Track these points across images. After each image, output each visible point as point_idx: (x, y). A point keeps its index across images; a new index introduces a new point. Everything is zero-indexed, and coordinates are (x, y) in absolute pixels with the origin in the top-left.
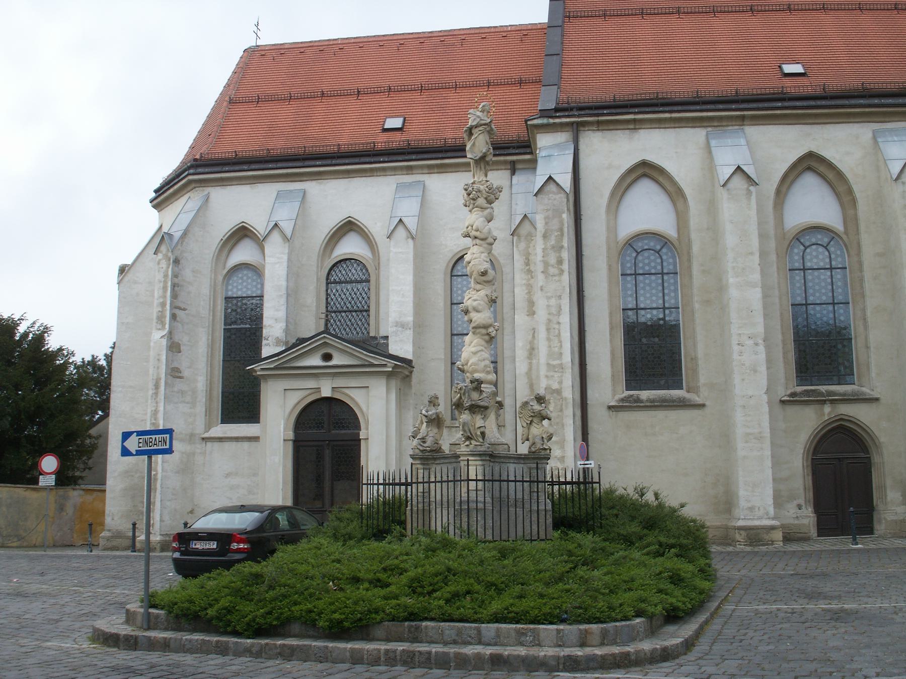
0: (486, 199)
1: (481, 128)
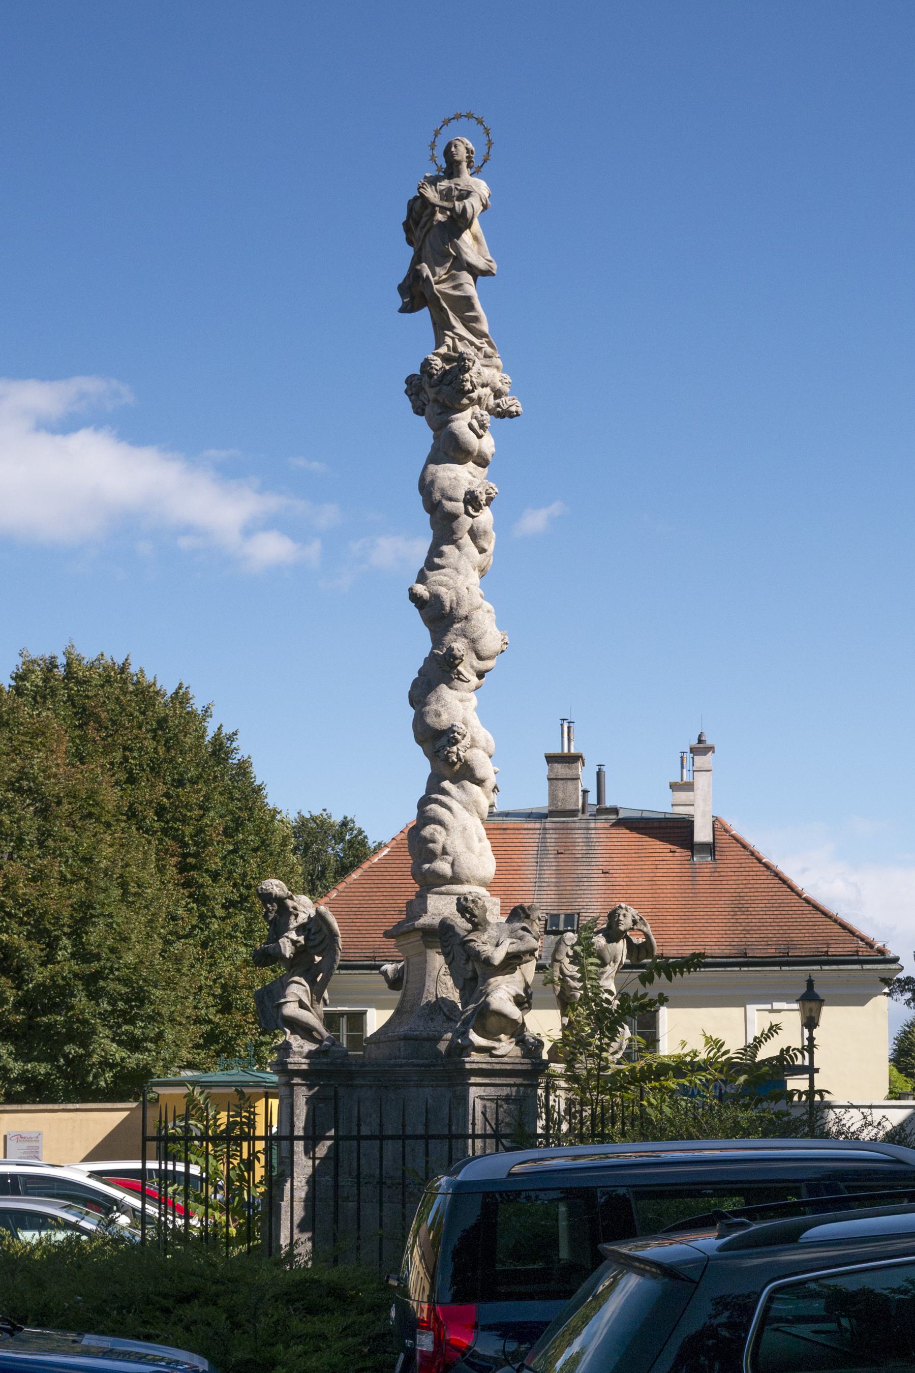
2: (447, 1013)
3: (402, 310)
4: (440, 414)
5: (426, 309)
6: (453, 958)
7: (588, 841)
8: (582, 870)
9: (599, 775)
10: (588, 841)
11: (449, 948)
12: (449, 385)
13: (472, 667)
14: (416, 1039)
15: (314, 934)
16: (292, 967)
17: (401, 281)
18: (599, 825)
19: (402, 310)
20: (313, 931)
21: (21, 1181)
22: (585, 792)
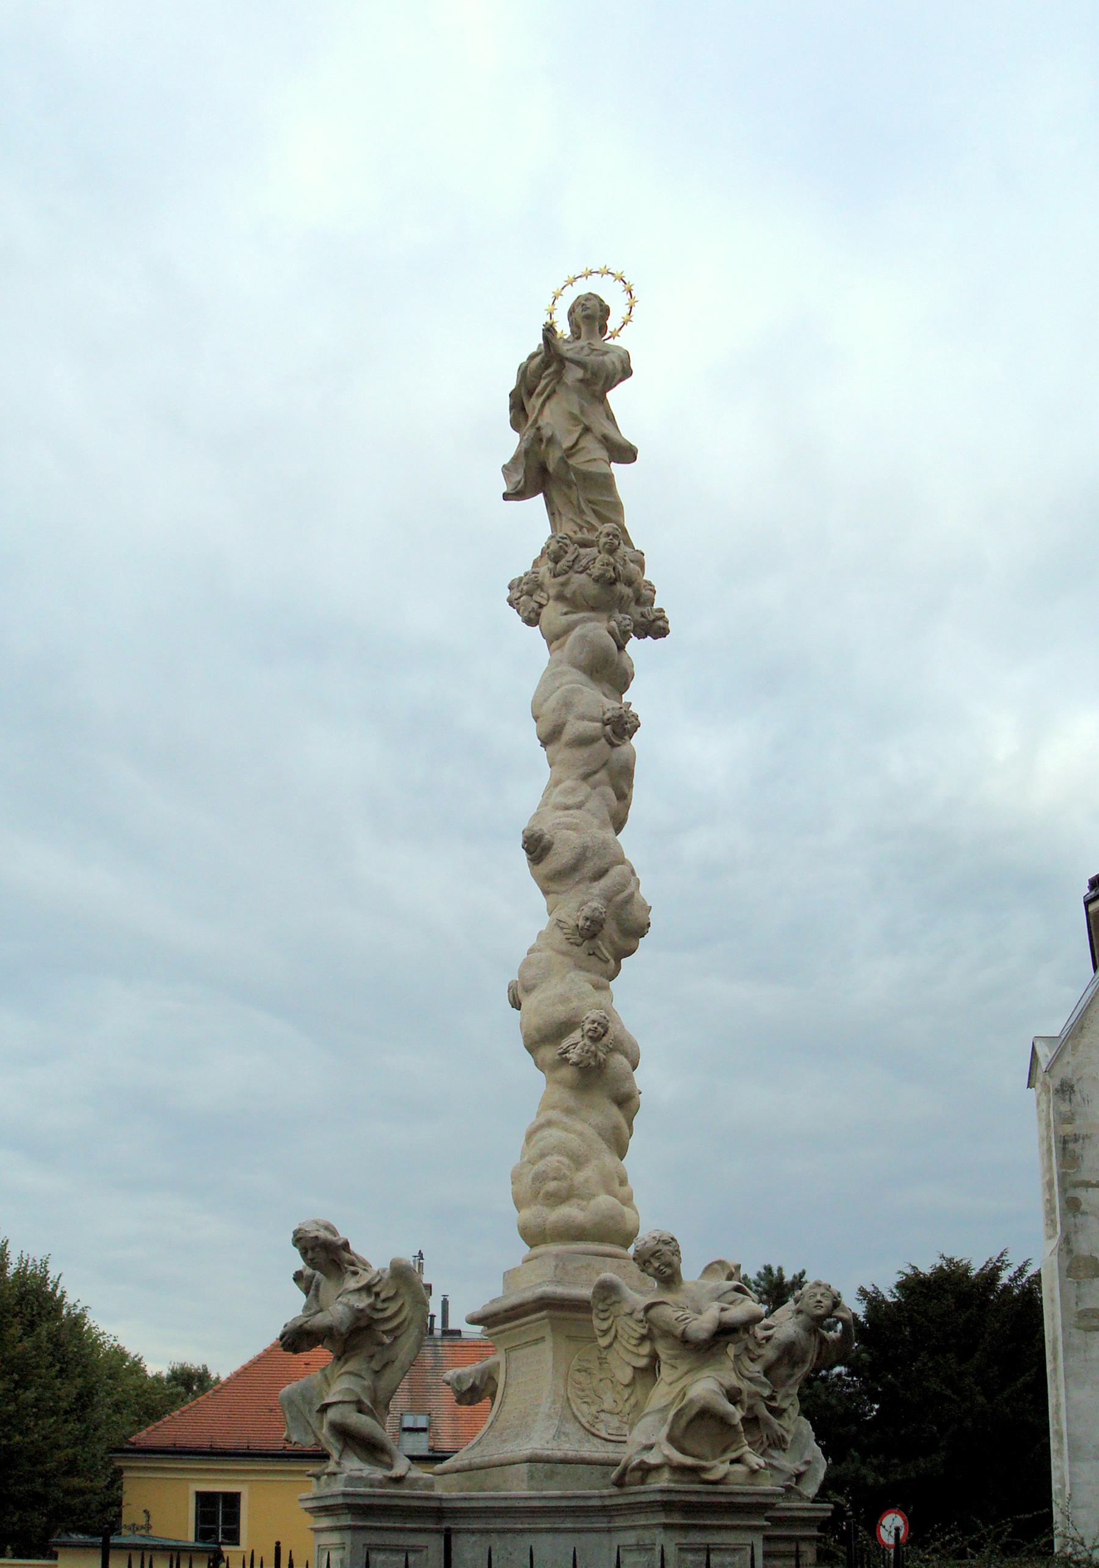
0: (560, 597)
2: (587, 1425)
3: (506, 497)
4: (566, 614)
5: (541, 495)
6: (616, 1337)
7: (436, 1355)
8: (430, 1379)
9: (445, 1304)
10: (436, 1355)
11: (610, 1321)
12: (581, 572)
13: (612, 943)
14: (547, 1461)
15: (384, 1301)
16: (345, 1352)
17: (507, 461)
18: (446, 1343)
19: (506, 497)
20: (383, 1296)
21: (10, 1554)
22: (433, 1316)
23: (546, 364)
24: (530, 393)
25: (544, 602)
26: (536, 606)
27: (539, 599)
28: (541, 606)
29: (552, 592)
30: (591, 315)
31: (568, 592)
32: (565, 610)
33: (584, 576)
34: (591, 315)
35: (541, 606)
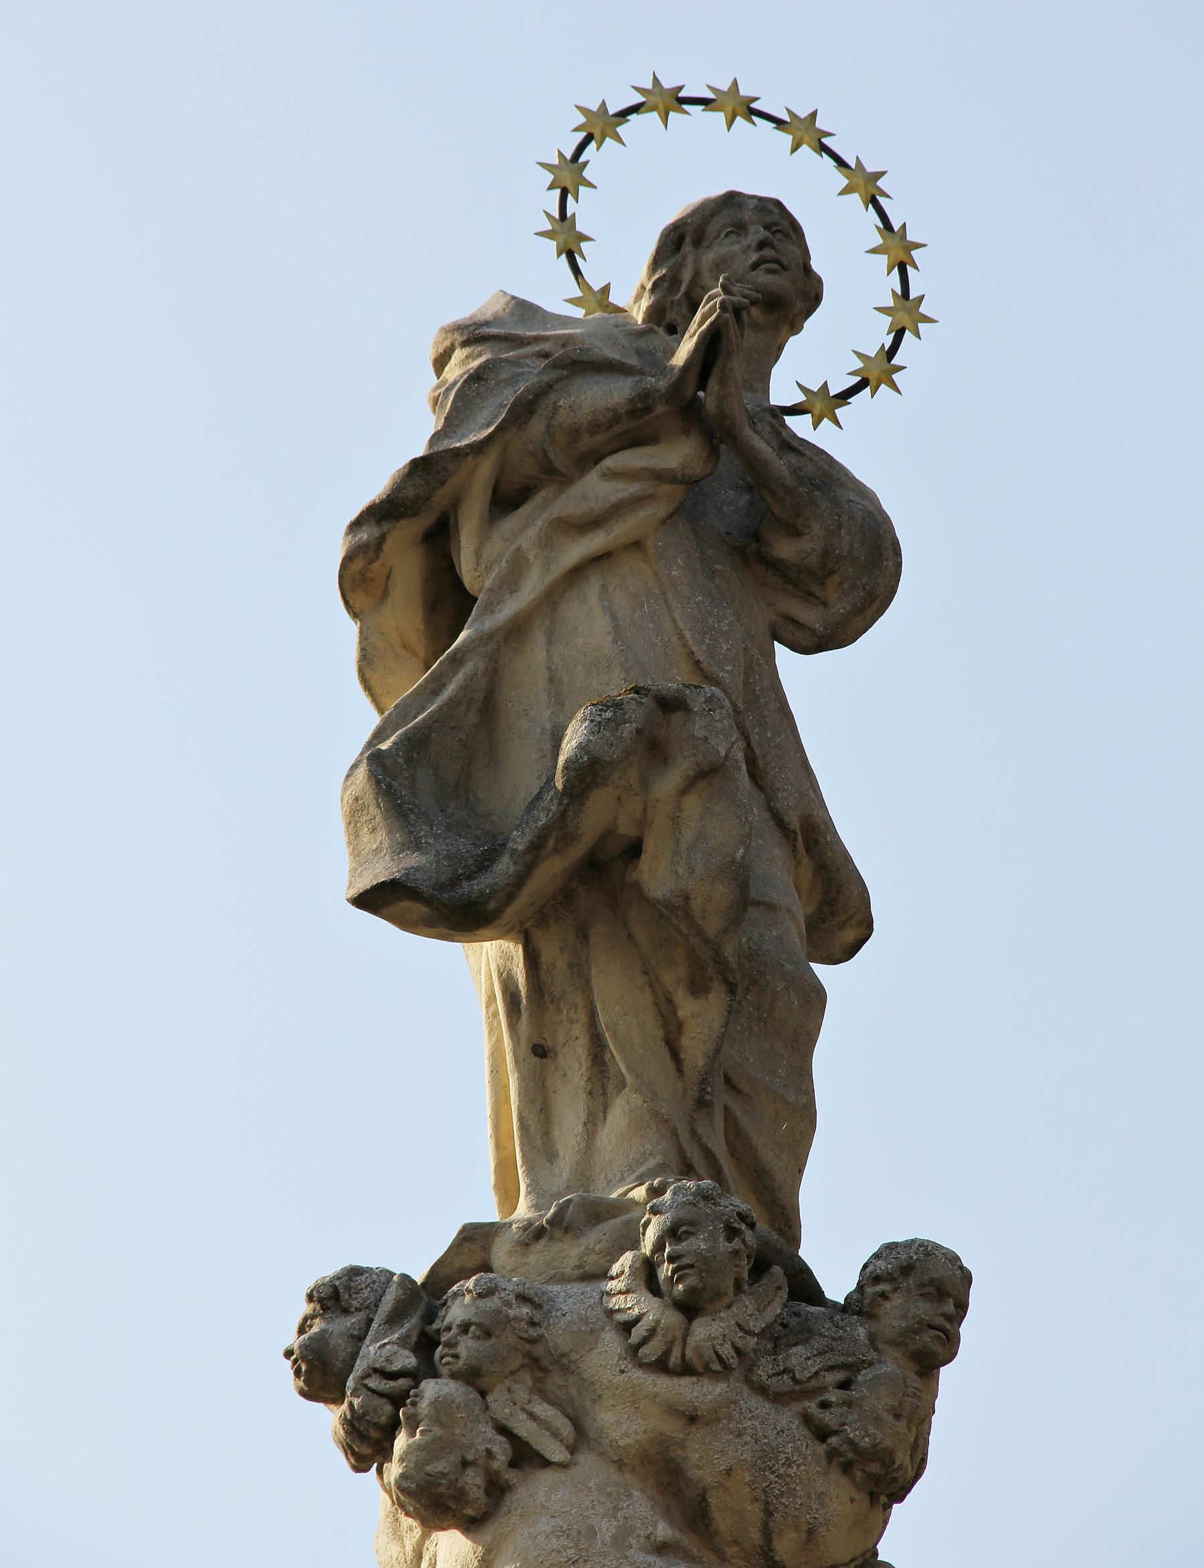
1: (594, 489)
12: (778, 1399)
23: (633, 427)
24: (505, 501)
25: (556, 1453)
26: (501, 1450)
27: (524, 1428)
28: (525, 1456)
29: (620, 1425)
30: (743, 266)
31: (705, 1458)
32: (664, 1531)
33: (787, 1419)
34: (743, 266)
35: (525, 1456)
